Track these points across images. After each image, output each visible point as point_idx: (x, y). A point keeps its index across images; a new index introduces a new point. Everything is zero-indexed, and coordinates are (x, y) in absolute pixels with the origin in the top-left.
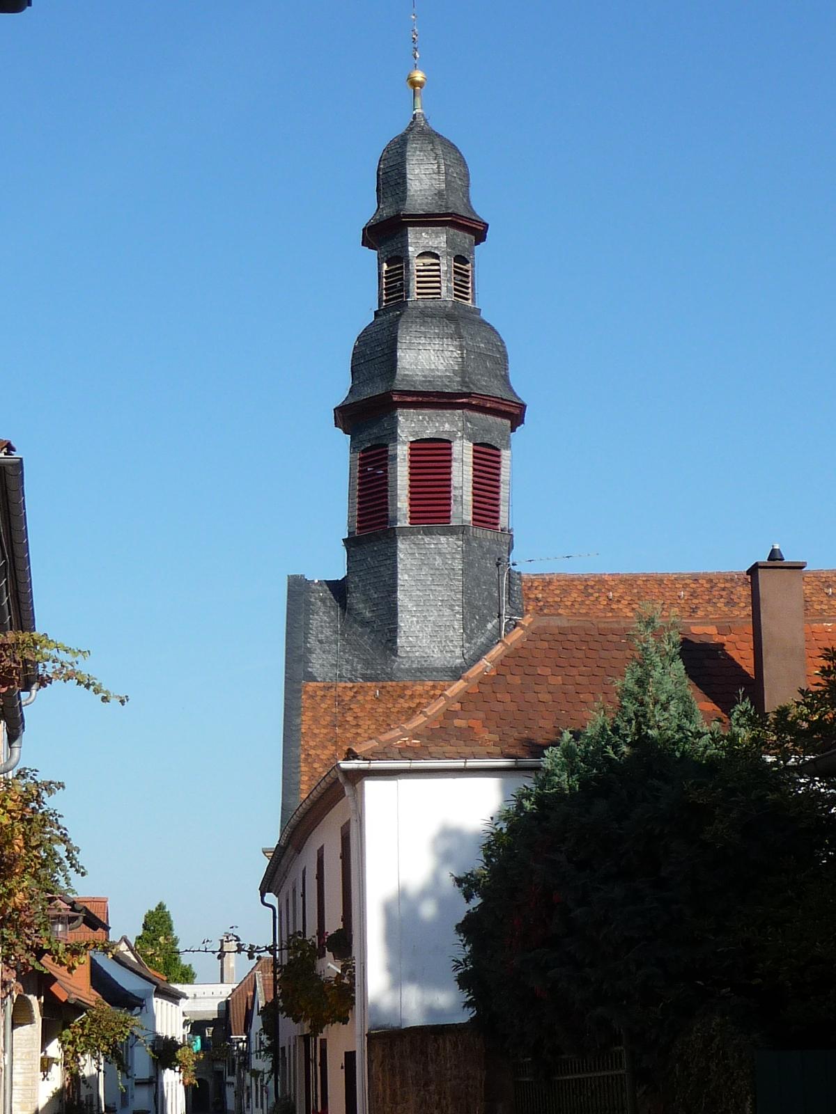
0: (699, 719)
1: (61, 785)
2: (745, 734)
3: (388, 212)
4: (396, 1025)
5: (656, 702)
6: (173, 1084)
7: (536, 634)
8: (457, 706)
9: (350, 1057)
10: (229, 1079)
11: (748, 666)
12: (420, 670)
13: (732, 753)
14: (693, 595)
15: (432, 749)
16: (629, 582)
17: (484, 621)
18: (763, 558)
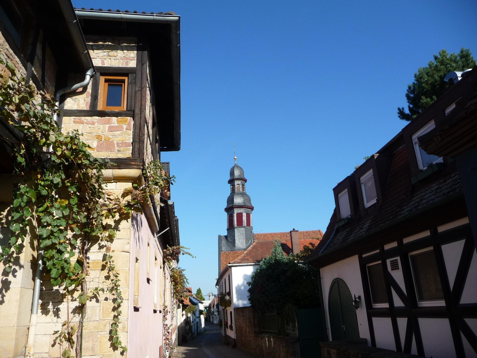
0: (284, 256)
1: (185, 270)
2: (292, 258)
3: (232, 178)
4: (238, 306)
5: (278, 253)
6: (202, 317)
7: (258, 243)
8: (246, 255)
9: (231, 312)
10: (211, 316)
11: (291, 247)
12: (239, 249)
13: (290, 261)
14: (281, 236)
15: (242, 262)
16: (271, 234)
17: (249, 241)
18: (292, 230)
